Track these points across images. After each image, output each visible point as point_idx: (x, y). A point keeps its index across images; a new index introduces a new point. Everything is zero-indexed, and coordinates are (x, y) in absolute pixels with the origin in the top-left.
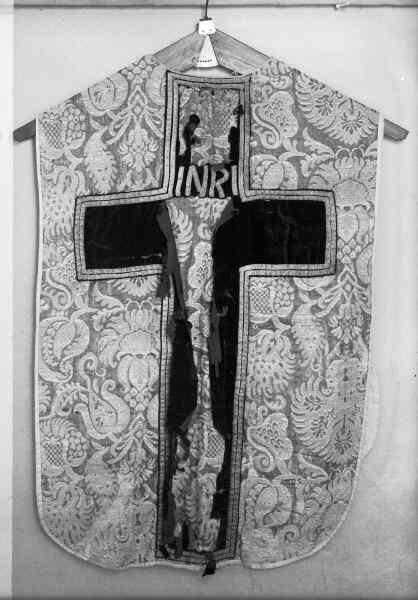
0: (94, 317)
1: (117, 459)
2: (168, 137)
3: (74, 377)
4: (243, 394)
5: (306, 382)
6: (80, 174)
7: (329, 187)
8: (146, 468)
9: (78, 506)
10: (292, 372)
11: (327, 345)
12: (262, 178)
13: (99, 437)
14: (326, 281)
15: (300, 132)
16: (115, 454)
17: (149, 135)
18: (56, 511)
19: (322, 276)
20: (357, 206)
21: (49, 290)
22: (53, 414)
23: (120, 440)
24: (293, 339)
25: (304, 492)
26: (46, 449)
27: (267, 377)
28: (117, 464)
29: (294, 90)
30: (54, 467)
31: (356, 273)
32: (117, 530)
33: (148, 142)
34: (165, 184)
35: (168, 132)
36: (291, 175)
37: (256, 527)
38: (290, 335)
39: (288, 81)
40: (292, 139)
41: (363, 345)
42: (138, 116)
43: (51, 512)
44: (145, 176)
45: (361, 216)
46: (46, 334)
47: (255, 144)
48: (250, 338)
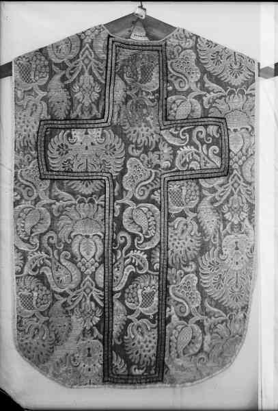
0: (53, 206)
1: (72, 307)
2: (108, 84)
3: (40, 247)
4: (165, 263)
5: (209, 251)
6: (44, 104)
7: (222, 116)
8: (94, 91)
9: (44, 338)
10: (199, 245)
11: (222, 225)
12: (175, 112)
13: (59, 290)
14: (221, 180)
15: (202, 78)
16: (71, 303)
17: (95, 81)
18: (27, 341)
19: (219, 177)
20: (243, 128)
21: (20, 186)
22: (25, 273)
23: (223, 190)
24: (198, 223)
25: (210, 328)
27: (182, 249)
28: (72, 311)
29: (196, 48)
30: (27, 311)
31: (242, 175)
32: (72, 358)
33: (93, 85)
34: (106, 116)
35: (108, 79)
36: (197, 108)
37: (178, 357)
38: (197, 220)
39: (192, 43)
40: (197, 83)
41: (250, 226)
42: (235, 189)
43: (24, 342)
44: (90, 110)
45: (245, 135)
46: (19, 217)
47: (170, 88)
48: (170, 224)
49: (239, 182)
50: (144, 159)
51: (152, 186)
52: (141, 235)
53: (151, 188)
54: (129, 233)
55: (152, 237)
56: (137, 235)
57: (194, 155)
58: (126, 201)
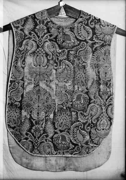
6: (56, 127)
23: (43, 140)
26: (70, 40)
38: (55, 129)
42: (37, 140)
48: (71, 62)
49: (38, 42)
50: (81, 61)
51: (74, 151)
52: (80, 130)
53: (74, 150)
54: (89, 26)
55: (75, 128)
56: (81, 129)
57: (59, 55)
58: (91, 42)
